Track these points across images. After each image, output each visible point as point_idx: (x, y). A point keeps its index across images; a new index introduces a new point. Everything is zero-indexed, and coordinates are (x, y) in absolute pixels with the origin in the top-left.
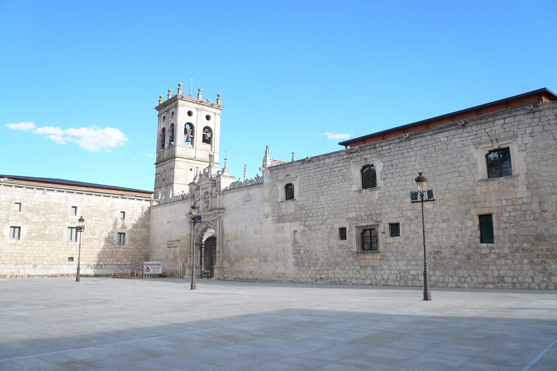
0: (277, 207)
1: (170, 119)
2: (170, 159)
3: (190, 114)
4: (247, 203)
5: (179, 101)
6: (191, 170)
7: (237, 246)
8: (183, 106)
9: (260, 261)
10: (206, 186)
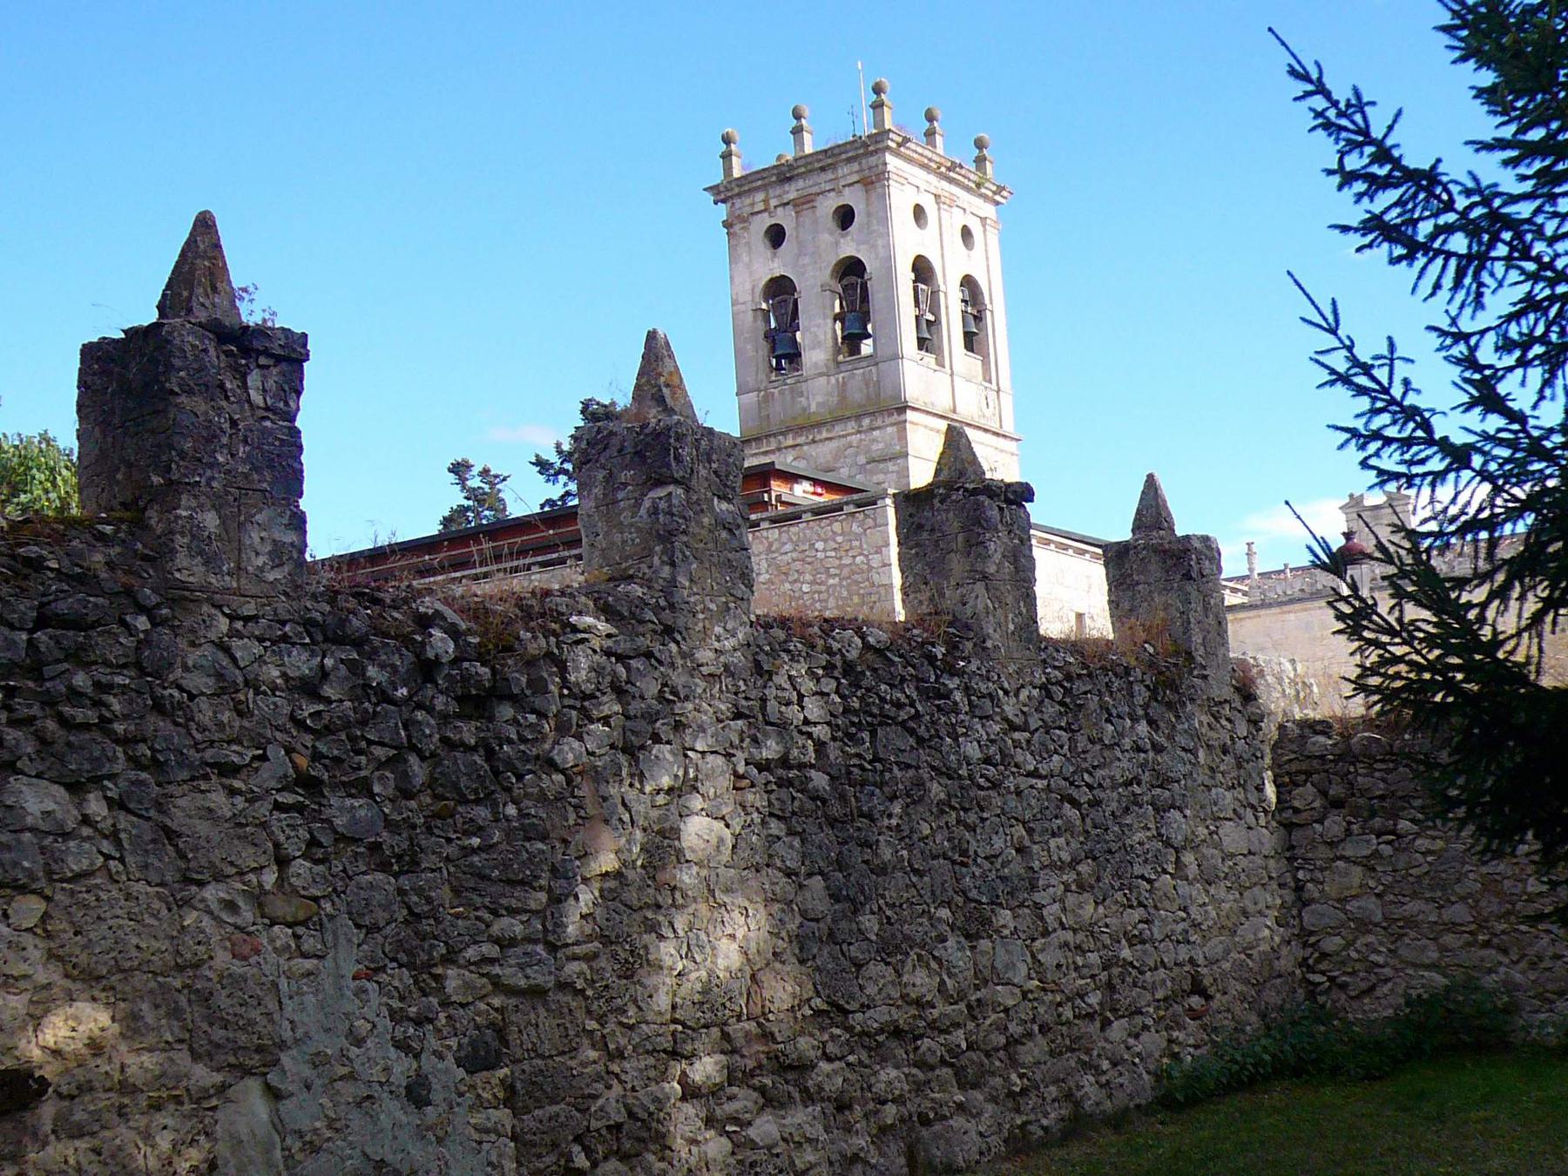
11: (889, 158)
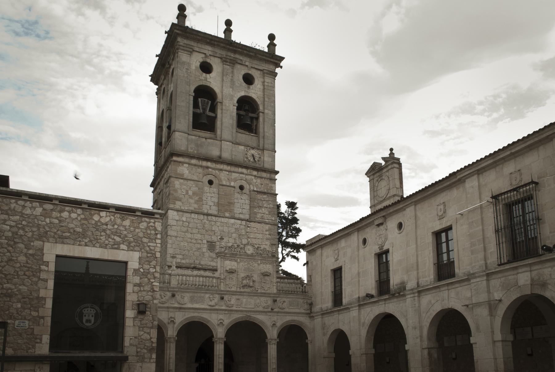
5: (179, 39)
6: (211, 182)
8: (191, 51)
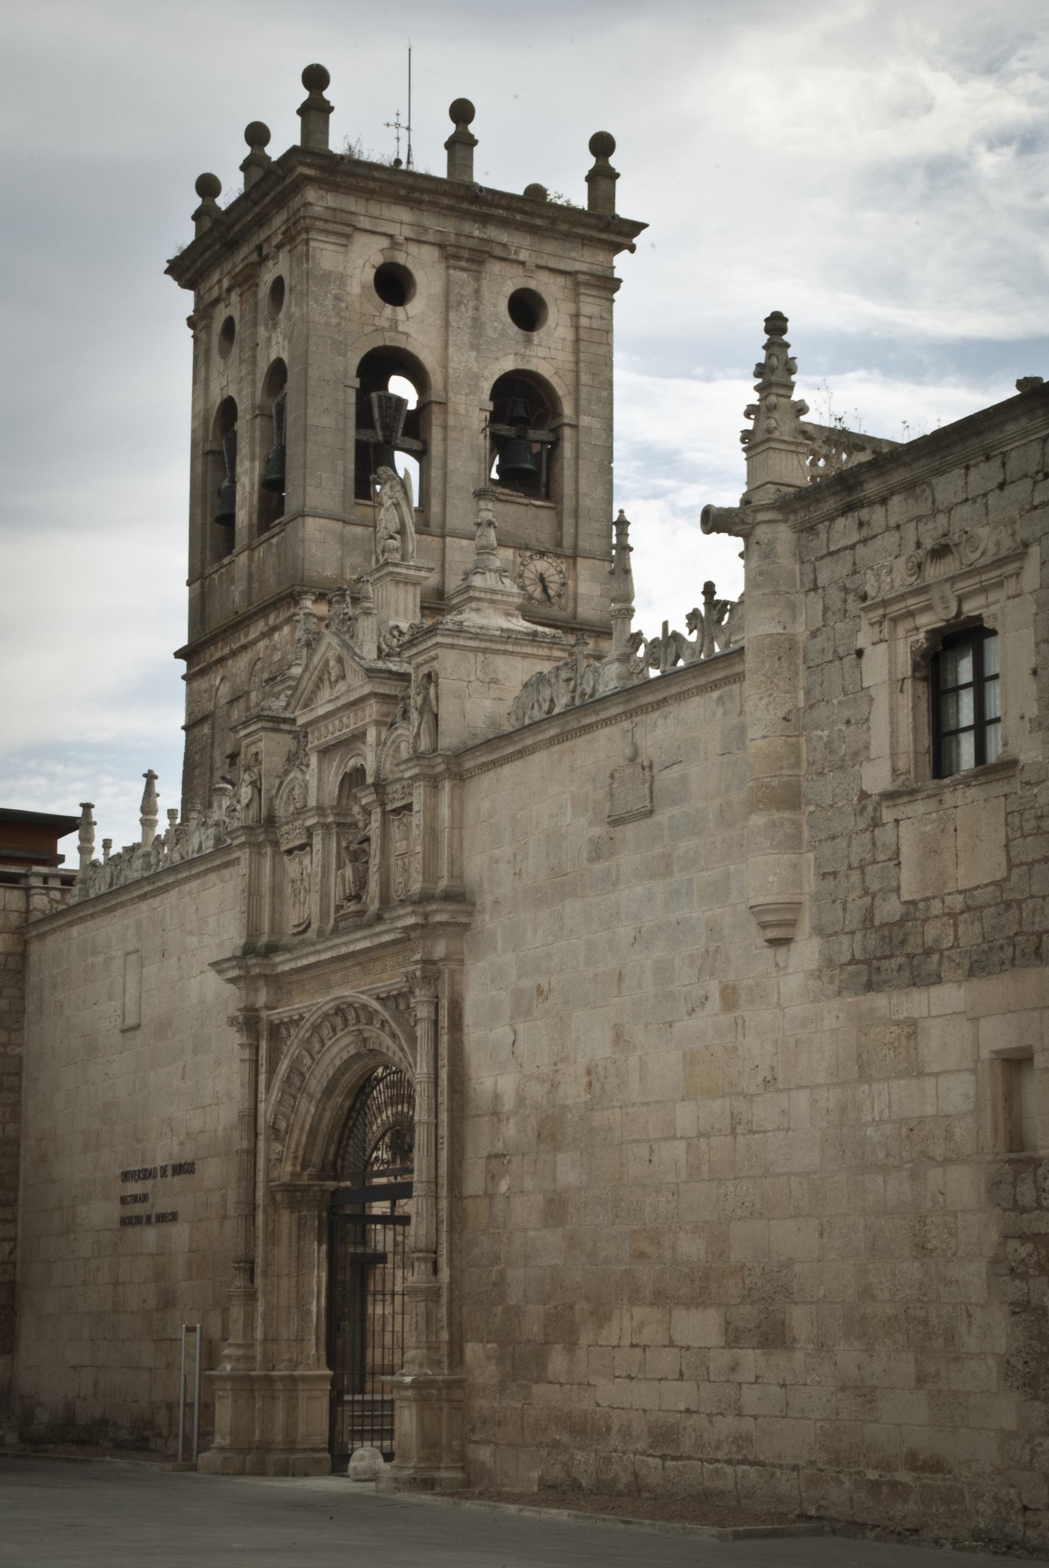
0: (858, 851)
1: (262, 332)
2: (264, 611)
3: (393, 285)
4: (629, 831)
7: (556, 1208)
8: (345, 231)
9: (733, 1338)
10: (350, 723)
11: (311, 194)
